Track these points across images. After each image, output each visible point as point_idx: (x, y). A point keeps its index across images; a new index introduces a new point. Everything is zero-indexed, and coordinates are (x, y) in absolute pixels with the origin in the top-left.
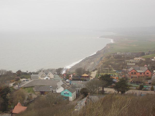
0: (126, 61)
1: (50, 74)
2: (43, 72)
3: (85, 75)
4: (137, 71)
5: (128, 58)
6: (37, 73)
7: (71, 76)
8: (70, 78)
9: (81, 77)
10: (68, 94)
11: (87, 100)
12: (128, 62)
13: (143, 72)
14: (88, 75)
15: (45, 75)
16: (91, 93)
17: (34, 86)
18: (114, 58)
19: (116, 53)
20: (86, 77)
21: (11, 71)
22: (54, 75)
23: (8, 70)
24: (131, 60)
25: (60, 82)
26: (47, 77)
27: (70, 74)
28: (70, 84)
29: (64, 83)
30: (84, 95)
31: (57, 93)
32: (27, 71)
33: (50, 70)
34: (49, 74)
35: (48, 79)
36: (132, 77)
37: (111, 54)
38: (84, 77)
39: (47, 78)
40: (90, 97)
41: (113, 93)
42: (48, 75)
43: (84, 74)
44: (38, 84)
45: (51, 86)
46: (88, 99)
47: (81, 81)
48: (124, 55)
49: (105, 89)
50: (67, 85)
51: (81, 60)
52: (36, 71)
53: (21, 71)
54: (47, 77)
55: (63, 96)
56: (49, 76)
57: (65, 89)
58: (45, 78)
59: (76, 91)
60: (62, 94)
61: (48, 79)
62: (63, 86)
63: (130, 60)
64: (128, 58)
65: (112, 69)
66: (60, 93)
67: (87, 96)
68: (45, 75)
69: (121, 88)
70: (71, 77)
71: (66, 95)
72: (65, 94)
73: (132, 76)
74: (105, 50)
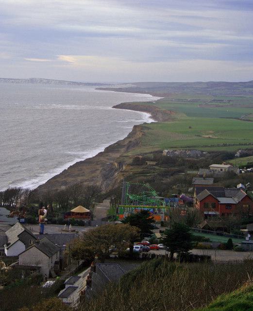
4: (219, 199)
5: (194, 166)
12: (195, 176)
13: (235, 203)
18: (156, 165)
19: (162, 152)
20: (82, 214)
24: (202, 171)
25: (16, 226)
30: (139, 232)
31: (8, 257)
36: (206, 216)
37: (138, 155)
40: (102, 267)
41: (190, 235)
43: (76, 206)
47: (70, 226)
48: (92, 186)
59: (59, 253)
63: (200, 169)
64: (194, 166)
65: (154, 193)
70: (42, 214)
73: (205, 213)
74: (131, 142)
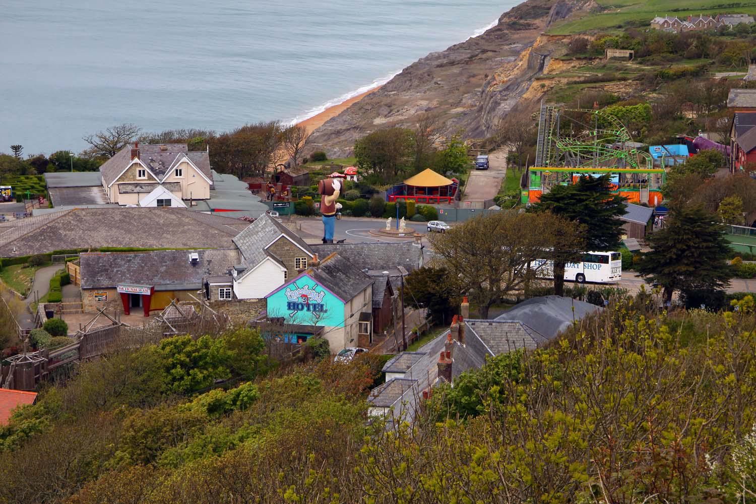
0: (719, 76)
1: (184, 168)
2: (135, 154)
3: (429, 178)
6: (87, 165)
7: (336, 185)
8: (327, 199)
9: (402, 190)
10: (319, 308)
11: (455, 352)
14: (447, 182)
15: (150, 178)
16: (475, 300)
17: (75, 252)
20: (432, 190)
21: (67, 329)
22: (211, 177)
23: (240, 126)
26: (160, 193)
27: (326, 175)
28: (325, 241)
29: (284, 230)
32: (16, 148)
33: (179, 141)
34: (178, 172)
35: (168, 202)
38: (421, 190)
39: (164, 197)
40: (480, 328)
42: (170, 177)
43: (419, 169)
44: (101, 238)
45: (195, 256)
46: (460, 339)
49: (571, 272)
50: (309, 247)
51: (392, 77)
52: (81, 151)
53: (239, 178)
54: (160, 193)
55: (279, 321)
56: (173, 186)
57: (289, 278)
58: (149, 200)
59: (369, 291)
60: (277, 308)
61: (168, 202)
62: (277, 253)
66: (263, 302)
67: (453, 325)
68: (150, 178)
69: (683, 269)
70: (331, 191)
71: (304, 318)
72: (292, 306)
